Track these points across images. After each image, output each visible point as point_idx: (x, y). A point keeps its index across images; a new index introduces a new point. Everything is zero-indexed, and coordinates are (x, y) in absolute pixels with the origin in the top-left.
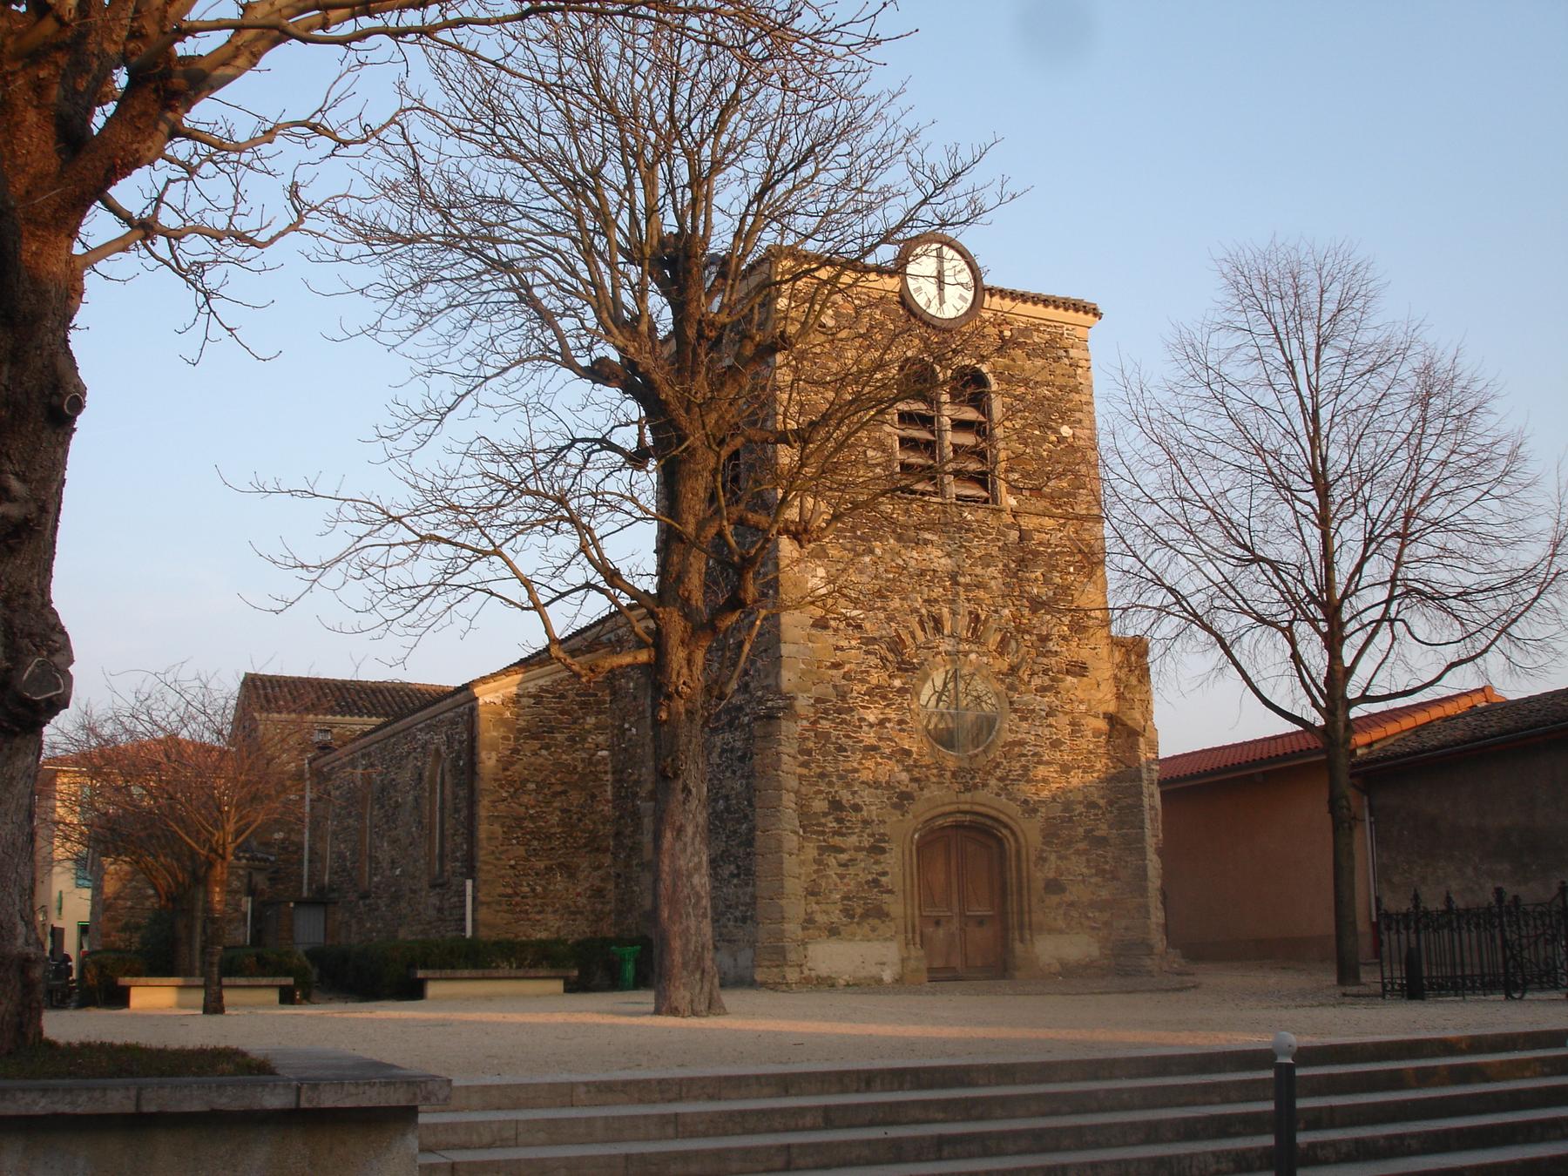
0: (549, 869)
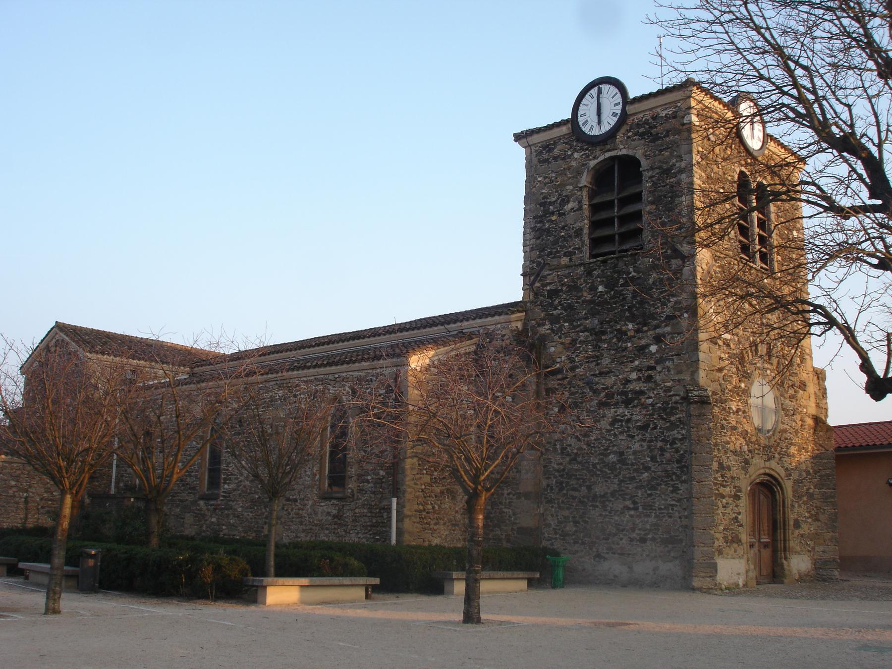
0: (442, 492)
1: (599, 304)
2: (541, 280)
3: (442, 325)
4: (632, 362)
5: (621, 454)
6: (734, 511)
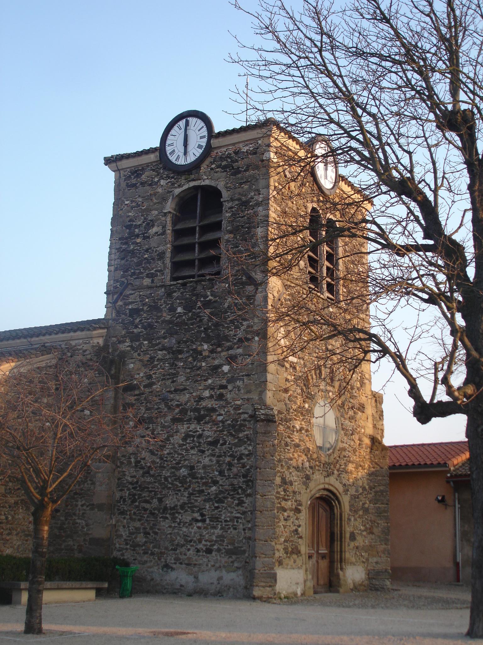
0: (16, 503)
1: (177, 324)
2: (124, 299)
3: (25, 338)
4: (205, 380)
5: (192, 468)
6: (292, 524)
